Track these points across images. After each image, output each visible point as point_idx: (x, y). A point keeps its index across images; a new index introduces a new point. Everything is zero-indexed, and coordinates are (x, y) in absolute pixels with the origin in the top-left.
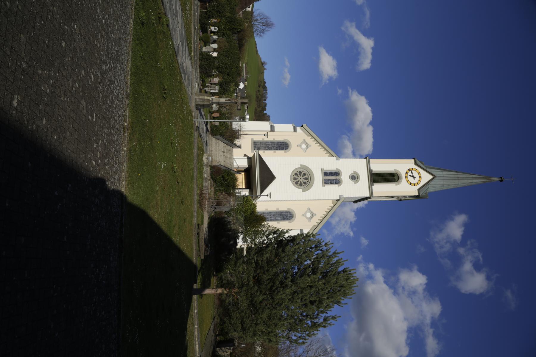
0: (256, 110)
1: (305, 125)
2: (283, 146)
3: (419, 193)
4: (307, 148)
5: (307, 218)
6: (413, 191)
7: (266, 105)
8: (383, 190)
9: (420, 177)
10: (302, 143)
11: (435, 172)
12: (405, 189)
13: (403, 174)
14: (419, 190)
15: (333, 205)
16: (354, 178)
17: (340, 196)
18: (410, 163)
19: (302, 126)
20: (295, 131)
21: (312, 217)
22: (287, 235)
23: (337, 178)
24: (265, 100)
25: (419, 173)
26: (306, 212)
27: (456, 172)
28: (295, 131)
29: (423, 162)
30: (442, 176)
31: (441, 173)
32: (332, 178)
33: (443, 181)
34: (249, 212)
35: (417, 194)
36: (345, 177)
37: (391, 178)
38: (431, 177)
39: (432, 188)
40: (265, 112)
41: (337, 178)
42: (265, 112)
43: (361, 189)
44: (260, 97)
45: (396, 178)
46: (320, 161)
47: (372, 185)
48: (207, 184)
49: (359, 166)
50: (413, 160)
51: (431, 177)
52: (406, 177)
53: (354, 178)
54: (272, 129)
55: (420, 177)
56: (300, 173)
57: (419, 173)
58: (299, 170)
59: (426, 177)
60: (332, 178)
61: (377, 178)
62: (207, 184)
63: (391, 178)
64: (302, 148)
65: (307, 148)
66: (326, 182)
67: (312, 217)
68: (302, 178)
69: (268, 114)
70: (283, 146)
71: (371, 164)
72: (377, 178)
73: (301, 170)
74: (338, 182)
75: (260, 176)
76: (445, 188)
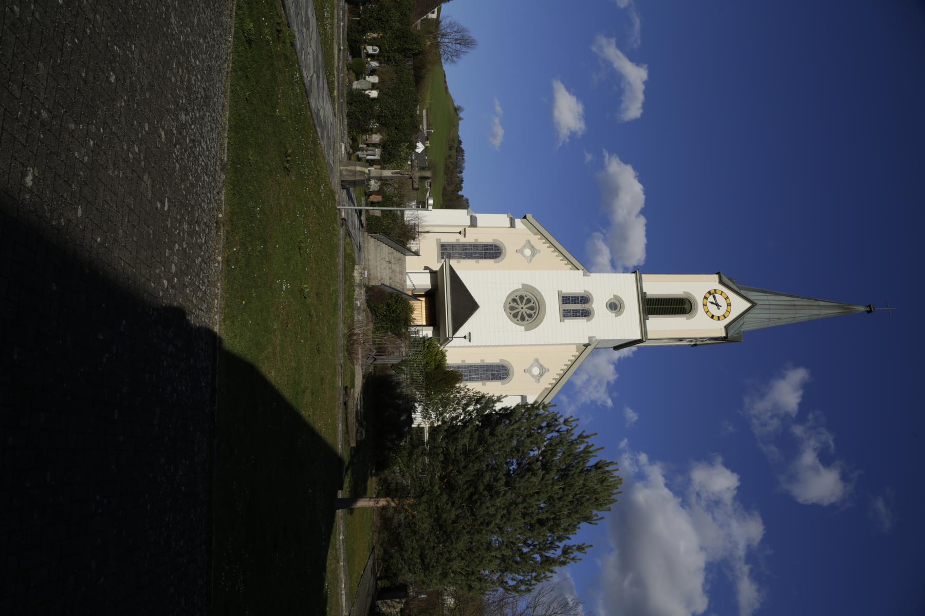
0: (445, 189)
1: (529, 216)
2: (491, 251)
3: (727, 332)
4: (533, 254)
5: (533, 376)
6: (717, 329)
7: (462, 181)
8: (664, 328)
9: (729, 305)
10: (524, 247)
11: (754, 296)
12: (702, 325)
13: (699, 300)
14: (727, 327)
15: (577, 354)
16: (615, 306)
17: (590, 338)
18: (711, 282)
19: (525, 217)
20: (512, 225)
21: (541, 375)
22: (498, 406)
23: (585, 306)
24: (461, 172)
25: (727, 298)
26: (532, 366)
27: (791, 296)
28: (512, 225)
29: (735, 280)
30: (767, 302)
31: (765, 298)
32: (576, 306)
33: (768, 311)
34: (433, 365)
35: (724, 335)
36: (598, 306)
37: (678, 306)
38: (748, 305)
39: (750, 325)
40: (460, 193)
41: (585, 306)
42: (460, 193)
43: (627, 326)
44: (451, 167)
45: (687, 306)
46: (555, 277)
47: (645, 319)
48: (360, 318)
49: (623, 285)
50: (717, 276)
51: (748, 305)
52: (705, 305)
53: (615, 306)
54: (473, 223)
55: (729, 305)
56: (521, 298)
57: (727, 298)
58: (519, 294)
59: (739, 305)
60: (576, 306)
61: (654, 306)
62: (360, 318)
63: (678, 306)
64: (524, 256)
65: (533, 254)
66: (566, 314)
67: (541, 375)
68: (525, 308)
69: (466, 196)
70: (491, 251)
71: (644, 283)
72: (654, 306)
73: (523, 293)
74: (586, 314)
75: (452, 303)
76: (772, 324)
